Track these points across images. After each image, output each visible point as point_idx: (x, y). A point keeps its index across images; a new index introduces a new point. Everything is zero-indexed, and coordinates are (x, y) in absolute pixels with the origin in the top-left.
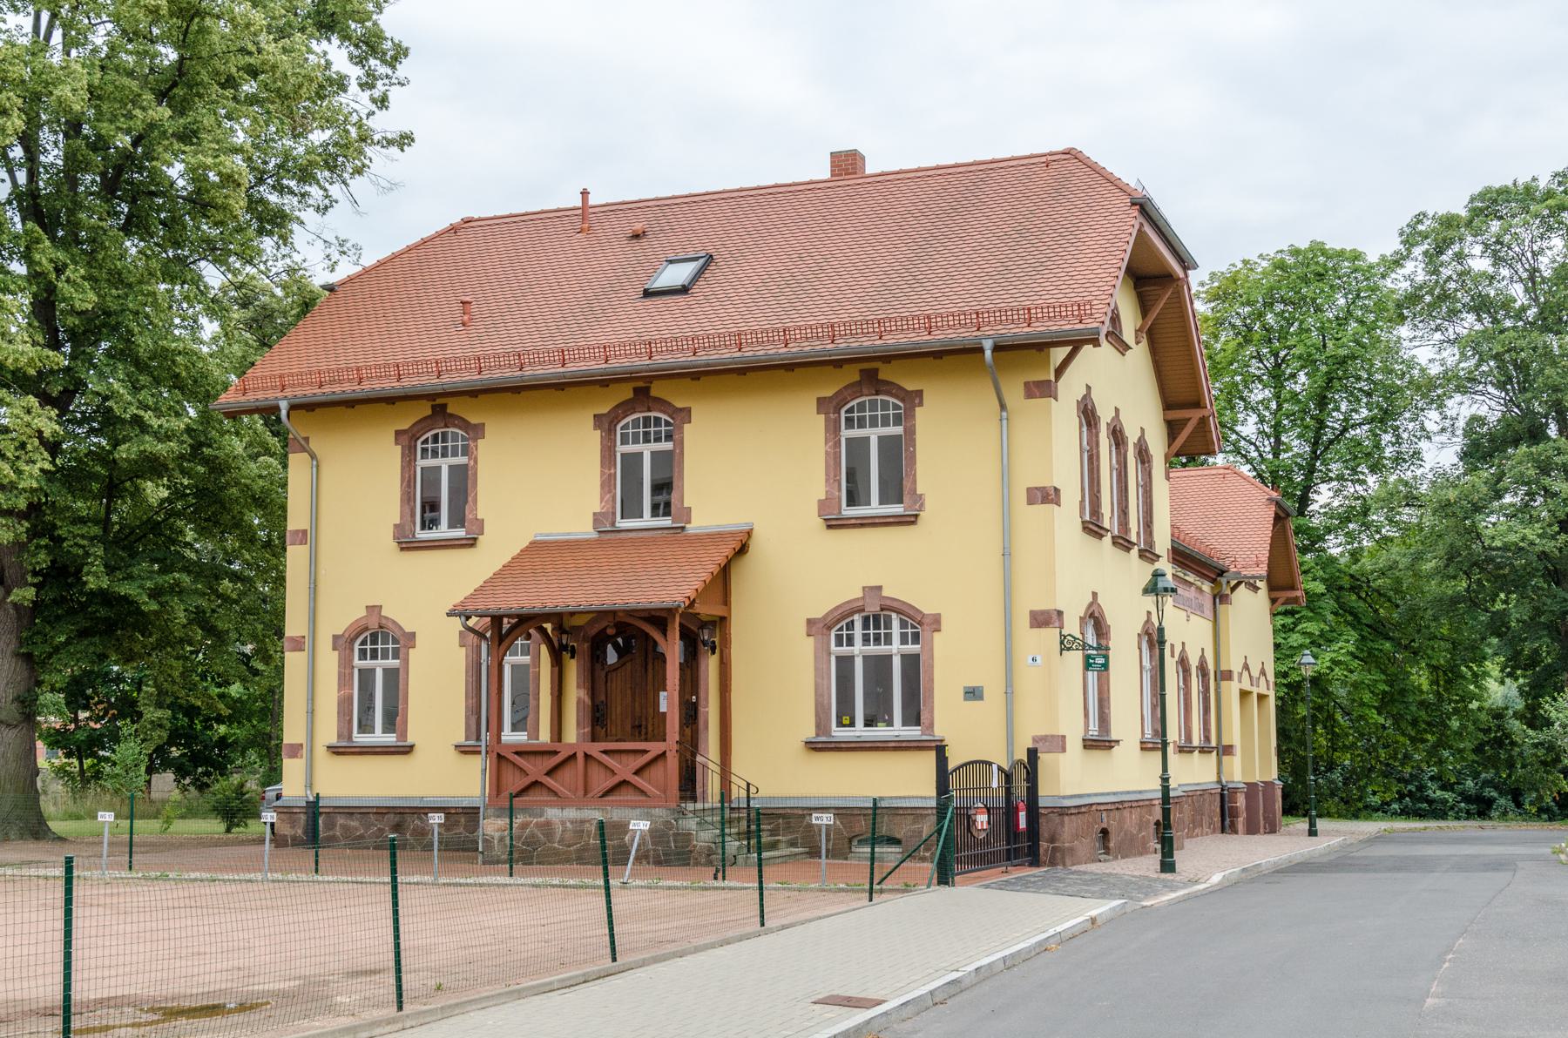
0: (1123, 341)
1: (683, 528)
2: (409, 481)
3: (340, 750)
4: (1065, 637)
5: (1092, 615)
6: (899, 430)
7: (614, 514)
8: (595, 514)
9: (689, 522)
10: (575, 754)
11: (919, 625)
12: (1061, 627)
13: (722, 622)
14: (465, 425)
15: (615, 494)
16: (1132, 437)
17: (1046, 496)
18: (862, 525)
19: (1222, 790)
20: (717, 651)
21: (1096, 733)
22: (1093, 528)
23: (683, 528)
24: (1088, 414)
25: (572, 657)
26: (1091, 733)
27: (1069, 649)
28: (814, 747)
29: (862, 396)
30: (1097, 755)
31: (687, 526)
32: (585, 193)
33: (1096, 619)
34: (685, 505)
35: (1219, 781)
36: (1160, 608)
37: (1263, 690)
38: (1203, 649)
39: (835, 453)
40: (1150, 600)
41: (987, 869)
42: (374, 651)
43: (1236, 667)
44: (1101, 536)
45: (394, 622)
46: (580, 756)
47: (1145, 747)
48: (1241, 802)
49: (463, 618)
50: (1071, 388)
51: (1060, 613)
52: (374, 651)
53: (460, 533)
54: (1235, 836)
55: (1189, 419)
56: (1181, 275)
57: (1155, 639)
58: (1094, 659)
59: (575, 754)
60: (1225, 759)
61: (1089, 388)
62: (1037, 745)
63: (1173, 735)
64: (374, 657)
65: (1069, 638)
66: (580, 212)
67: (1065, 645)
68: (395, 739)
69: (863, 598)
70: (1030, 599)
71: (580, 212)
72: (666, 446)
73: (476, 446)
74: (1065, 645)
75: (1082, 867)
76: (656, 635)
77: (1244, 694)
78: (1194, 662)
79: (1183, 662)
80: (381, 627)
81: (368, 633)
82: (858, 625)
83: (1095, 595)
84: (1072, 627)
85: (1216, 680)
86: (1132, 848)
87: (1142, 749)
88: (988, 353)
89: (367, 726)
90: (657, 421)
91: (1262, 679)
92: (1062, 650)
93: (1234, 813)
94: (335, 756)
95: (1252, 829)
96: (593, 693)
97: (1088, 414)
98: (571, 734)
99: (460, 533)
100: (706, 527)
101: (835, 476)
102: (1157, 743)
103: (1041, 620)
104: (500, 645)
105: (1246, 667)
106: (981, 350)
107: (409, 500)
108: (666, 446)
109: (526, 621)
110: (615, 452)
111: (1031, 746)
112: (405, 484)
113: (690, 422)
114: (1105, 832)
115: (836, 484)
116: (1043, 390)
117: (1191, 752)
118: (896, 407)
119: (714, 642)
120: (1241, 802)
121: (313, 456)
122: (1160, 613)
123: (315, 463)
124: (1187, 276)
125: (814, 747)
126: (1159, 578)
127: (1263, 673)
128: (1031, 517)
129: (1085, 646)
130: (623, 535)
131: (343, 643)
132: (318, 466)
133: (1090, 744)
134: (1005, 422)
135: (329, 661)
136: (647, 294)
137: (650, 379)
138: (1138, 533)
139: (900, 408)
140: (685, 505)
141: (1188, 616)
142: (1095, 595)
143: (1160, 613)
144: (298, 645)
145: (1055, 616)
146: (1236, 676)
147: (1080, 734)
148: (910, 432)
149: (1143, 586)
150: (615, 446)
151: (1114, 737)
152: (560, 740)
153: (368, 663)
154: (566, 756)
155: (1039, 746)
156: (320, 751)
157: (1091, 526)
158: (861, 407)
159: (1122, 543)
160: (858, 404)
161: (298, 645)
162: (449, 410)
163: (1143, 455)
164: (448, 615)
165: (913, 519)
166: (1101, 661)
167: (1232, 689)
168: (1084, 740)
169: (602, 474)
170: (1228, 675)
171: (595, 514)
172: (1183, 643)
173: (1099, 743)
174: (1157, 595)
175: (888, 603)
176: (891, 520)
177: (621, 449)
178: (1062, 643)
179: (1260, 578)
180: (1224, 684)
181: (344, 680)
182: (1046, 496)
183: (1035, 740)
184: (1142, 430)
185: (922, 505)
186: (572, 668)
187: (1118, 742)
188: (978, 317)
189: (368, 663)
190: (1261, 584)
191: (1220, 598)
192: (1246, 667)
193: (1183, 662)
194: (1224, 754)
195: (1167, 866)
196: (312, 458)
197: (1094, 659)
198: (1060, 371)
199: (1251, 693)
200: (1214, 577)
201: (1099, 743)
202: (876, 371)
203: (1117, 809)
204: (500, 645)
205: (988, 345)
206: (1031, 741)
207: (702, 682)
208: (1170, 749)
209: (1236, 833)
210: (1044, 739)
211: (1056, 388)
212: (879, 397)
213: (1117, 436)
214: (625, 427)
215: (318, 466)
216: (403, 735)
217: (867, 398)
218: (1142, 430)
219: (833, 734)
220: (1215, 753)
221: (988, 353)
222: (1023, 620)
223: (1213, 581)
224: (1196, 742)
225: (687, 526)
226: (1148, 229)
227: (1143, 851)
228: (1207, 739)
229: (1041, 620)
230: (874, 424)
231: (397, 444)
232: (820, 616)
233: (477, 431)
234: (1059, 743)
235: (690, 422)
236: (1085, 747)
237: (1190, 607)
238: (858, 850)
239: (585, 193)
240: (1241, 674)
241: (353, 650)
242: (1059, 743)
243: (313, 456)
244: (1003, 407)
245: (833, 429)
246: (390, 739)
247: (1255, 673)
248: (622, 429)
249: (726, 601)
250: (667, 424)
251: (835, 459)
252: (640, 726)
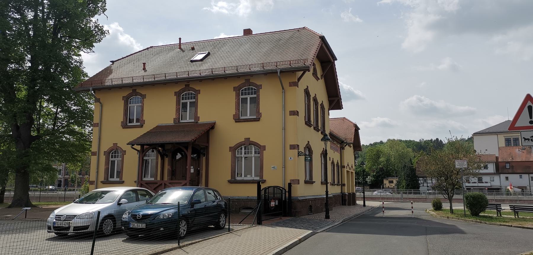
0: (318, 77)
1: (197, 122)
2: (126, 110)
3: (104, 182)
4: (299, 152)
5: (308, 147)
6: (255, 96)
7: (179, 118)
8: (174, 118)
9: (199, 121)
10: (162, 184)
11: (260, 149)
12: (298, 149)
13: (207, 148)
14: (141, 95)
15: (180, 113)
16: (320, 103)
17: (295, 113)
18: (245, 121)
19: (342, 195)
20: (205, 156)
21: (308, 179)
22: (308, 123)
23: (197, 122)
24: (307, 92)
25: (167, 157)
26: (307, 179)
27: (300, 155)
28: (230, 182)
29: (245, 86)
30: (309, 186)
31: (198, 122)
32: (180, 39)
33: (308, 147)
34: (198, 116)
35: (341, 193)
36: (326, 145)
37: (352, 171)
38: (338, 160)
39: (238, 102)
40: (323, 142)
41: (276, 218)
42: (115, 156)
43: (346, 165)
44: (310, 127)
45: (120, 148)
46: (163, 184)
47: (322, 183)
48: (347, 198)
49: (131, 145)
50: (303, 85)
51: (298, 146)
52: (115, 156)
53: (139, 124)
54: (345, 206)
55: (335, 100)
56: (333, 61)
57: (325, 154)
58: (307, 158)
59: (162, 184)
60: (343, 187)
61: (307, 87)
62: (291, 182)
63: (330, 180)
64: (115, 157)
65: (300, 152)
66: (179, 44)
67: (299, 154)
68: (119, 180)
69: (245, 141)
70: (291, 141)
71: (179, 44)
72: (194, 100)
73: (144, 100)
74: (299, 154)
75: (303, 217)
76: (185, 150)
77: (348, 172)
78: (336, 163)
79: (333, 163)
80: (117, 149)
81: (114, 151)
82: (243, 149)
83: (308, 142)
84: (302, 149)
85: (341, 168)
86: (318, 211)
87: (321, 184)
88: (279, 73)
89: (112, 176)
90: (192, 94)
91: (352, 168)
92: (298, 156)
93: (345, 200)
94: (103, 184)
95: (349, 205)
96: (172, 167)
97: (307, 92)
98: (166, 178)
99: (139, 124)
100: (203, 122)
101: (238, 108)
102: (325, 182)
103: (293, 147)
104: (143, 153)
105: (348, 165)
106: (277, 72)
107: (125, 115)
108: (194, 100)
109: (153, 146)
110: (180, 102)
111: (289, 182)
112: (125, 110)
113: (200, 94)
114: (311, 206)
115: (238, 110)
116: (295, 84)
117: (335, 185)
118: (255, 89)
119: (205, 153)
120: (347, 198)
121: (100, 103)
122: (326, 146)
123: (101, 105)
124: (334, 62)
125: (230, 182)
126: (326, 136)
127: (352, 167)
128: (291, 119)
129: (305, 155)
130: (181, 124)
131: (107, 154)
132: (102, 106)
133: (306, 182)
134: (283, 93)
135: (103, 158)
136: (192, 61)
137: (188, 82)
138: (321, 128)
139: (256, 90)
140: (198, 116)
141: (334, 152)
142: (308, 142)
143: (326, 146)
144: (94, 154)
145: (296, 146)
146: (346, 167)
147: (304, 179)
148: (258, 96)
149: (321, 138)
150: (180, 100)
151: (314, 180)
152: (163, 180)
153: (113, 159)
154: (159, 184)
155: (292, 182)
156: (99, 183)
157: (307, 123)
158: (245, 89)
159: (316, 129)
160: (245, 89)
161: (94, 154)
162: (137, 91)
163: (322, 105)
164: (127, 144)
165: (258, 119)
166: (309, 159)
167: (345, 170)
168: (305, 181)
169: (176, 108)
170: (344, 167)
171: (174, 118)
172: (333, 158)
173: (309, 182)
174: (325, 141)
175: (251, 142)
176: (252, 120)
177: (182, 101)
178: (298, 154)
179: (352, 143)
180: (343, 169)
181: (107, 163)
182: (295, 113)
183: (291, 180)
184: (322, 101)
185: (261, 116)
186: (167, 160)
187: (315, 182)
188: (276, 63)
189: (113, 159)
190: (352, 145)
191: (342, 148)
192: (348, 165)
193: (333, 163)
194: (343, 186)
195: (327, 217)
196: (100, 104)
197: (307, 158)
198: (299, 79)
199: (349, 171)
200: (341, 143)
201: (309, 182)
202: (249, 80)
203: (314, 200)
204: (143, 153)
205: (279, 71)
206: (289, 181)
207: (393, 216)
208: (329, 185)
209: (346, 205)
210: (293, 180)
211: (298, 84)
212: (250, 87)
213: (315, 100)
214: (183, 95)
215: (102, 106)
216: (121, 178)
217: (247, 87)
218: (322, 101)
219: (236, 179)
220: (340, 186)
221: (279, 73)
222: (288, 147)
223: (340, 144)
224: (336, 183)
225: (198, 122)
226: (323, 45)
227: (322, 211)
228: (339, 182)
229: (293, 147)
230: (249, 94)
231: (123, 100)
232: (233, 146)
233: (144, 97)
234: (298, 182)
235: (200, 94)
236: (305, 183)
237: (335, 150)
238: (242, 211)
239: (180, 39)
240: (347, 167)
241: (110, 155)
242: (298, 182)
243: (100, 103)
244: (283, 88)
245: (238, 96)
246: (118, 179)
247: (350, 167)
248: (182, 96)
249: (208, 142)
250: (194, 94)
251: (238, 103)
252: (184, 176)
